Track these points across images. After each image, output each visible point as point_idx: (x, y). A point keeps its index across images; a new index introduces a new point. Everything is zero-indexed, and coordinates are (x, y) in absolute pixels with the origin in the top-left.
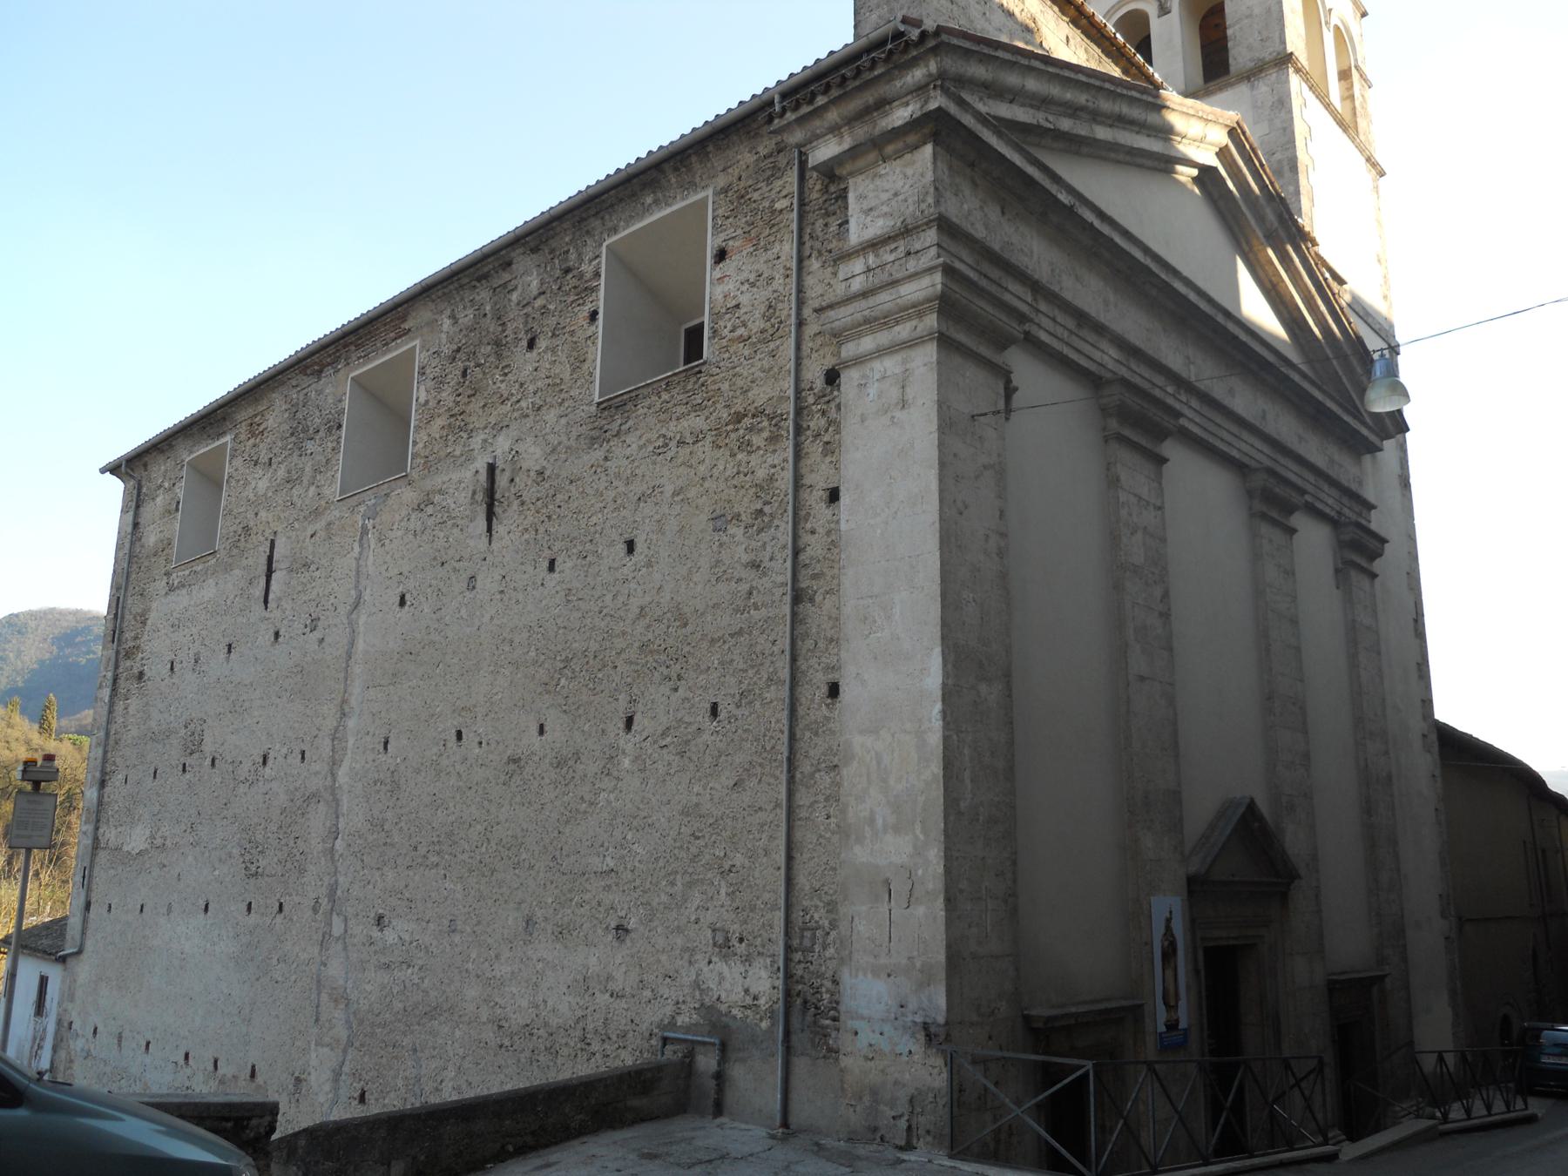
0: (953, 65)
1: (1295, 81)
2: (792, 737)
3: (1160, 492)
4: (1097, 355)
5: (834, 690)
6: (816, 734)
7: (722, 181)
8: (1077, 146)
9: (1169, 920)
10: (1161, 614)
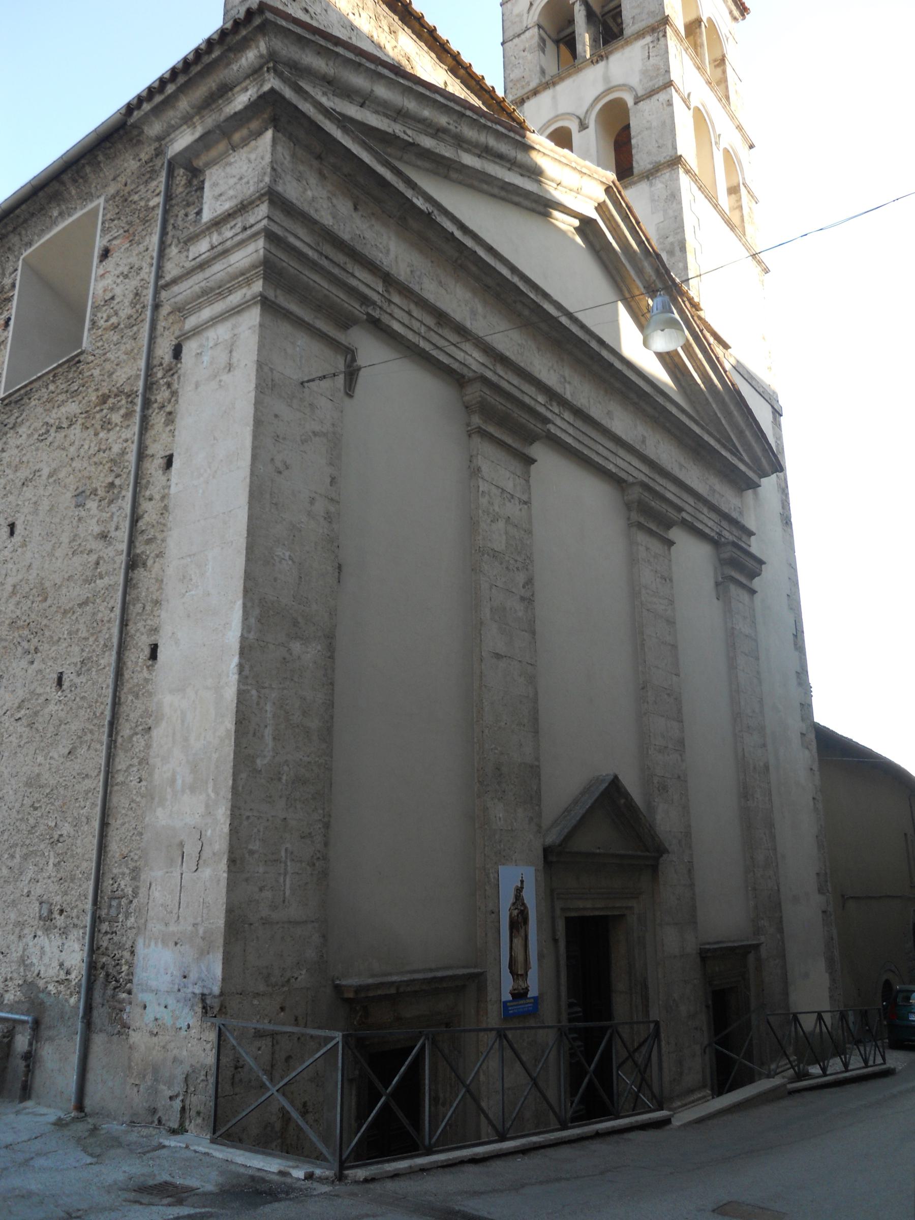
0: (288, 50)
1: (684, 180)
2: (116, 703)
3: (528, 488)
4: (460, 356)
5: (154, 654)
6: (137, 697)
7: (111, 190)
8: (445, 169)
9: (519, 890)
10: (523, 599)
